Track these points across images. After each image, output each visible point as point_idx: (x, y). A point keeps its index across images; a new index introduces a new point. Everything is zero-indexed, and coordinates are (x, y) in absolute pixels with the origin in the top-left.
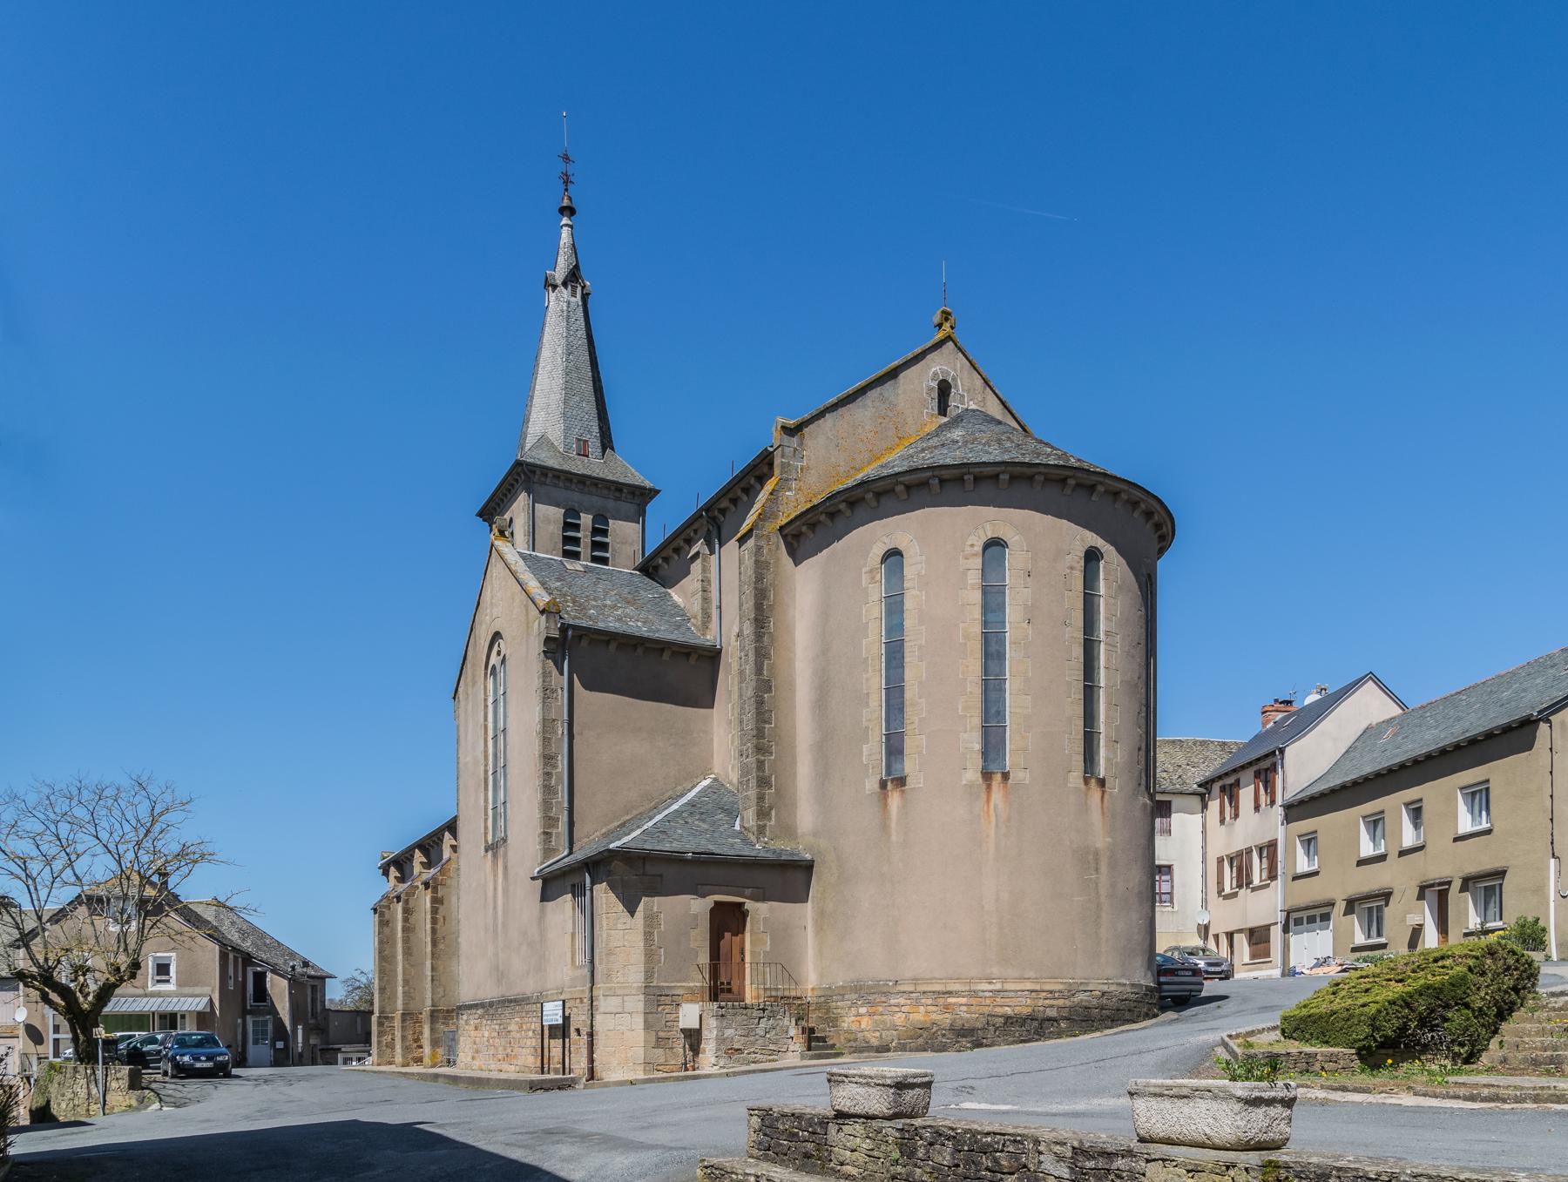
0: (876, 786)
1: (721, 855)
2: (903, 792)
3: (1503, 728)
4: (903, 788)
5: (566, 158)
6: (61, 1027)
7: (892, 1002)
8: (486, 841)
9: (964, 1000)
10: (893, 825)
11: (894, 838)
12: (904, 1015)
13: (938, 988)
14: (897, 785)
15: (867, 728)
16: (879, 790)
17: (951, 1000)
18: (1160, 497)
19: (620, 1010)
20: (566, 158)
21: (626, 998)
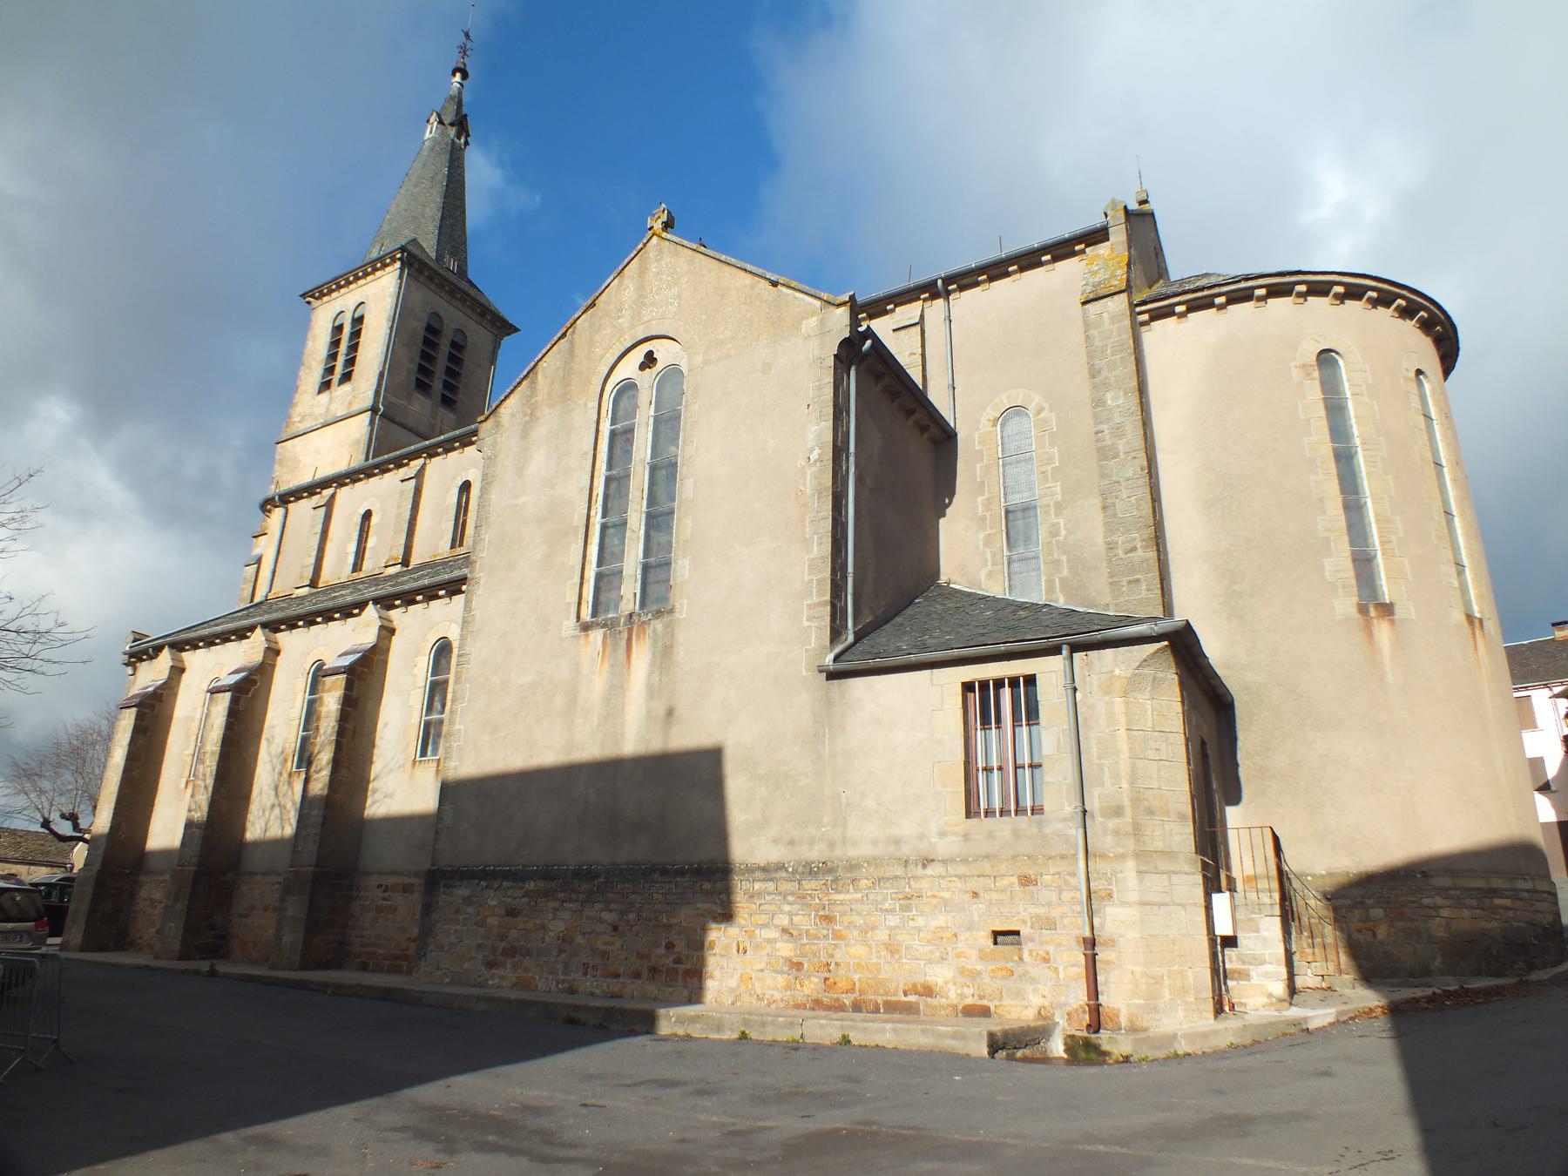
0: (1353, 611)
1: (205, 700)
2: (1392, 622)
3: (249, 670)
4: (1391, 617)
5: (467, 35)
6: (995, 929)
7: (1426, 901)
8: (664, 654)
9: (1508, 902)
10: (1387, 661)
11: (1390, 678)
12: (1444, 922)
13: (1481, 884)
14: (1384, 612)
15: (1327, 539)
16: (1358, 616)
17: (1498, 901)
18: (1449, 313)
19: (1167, 899)
20: (467, 35)
21: (1175, 878)
